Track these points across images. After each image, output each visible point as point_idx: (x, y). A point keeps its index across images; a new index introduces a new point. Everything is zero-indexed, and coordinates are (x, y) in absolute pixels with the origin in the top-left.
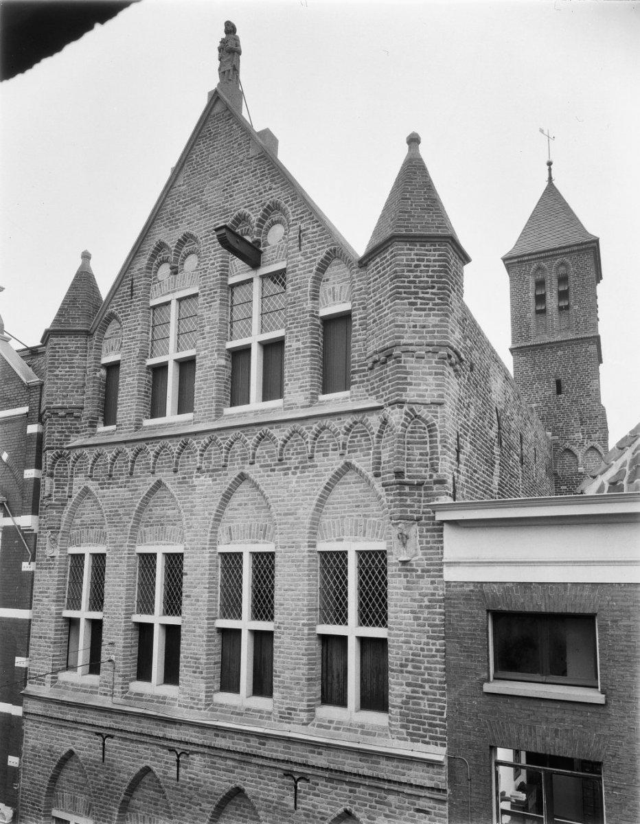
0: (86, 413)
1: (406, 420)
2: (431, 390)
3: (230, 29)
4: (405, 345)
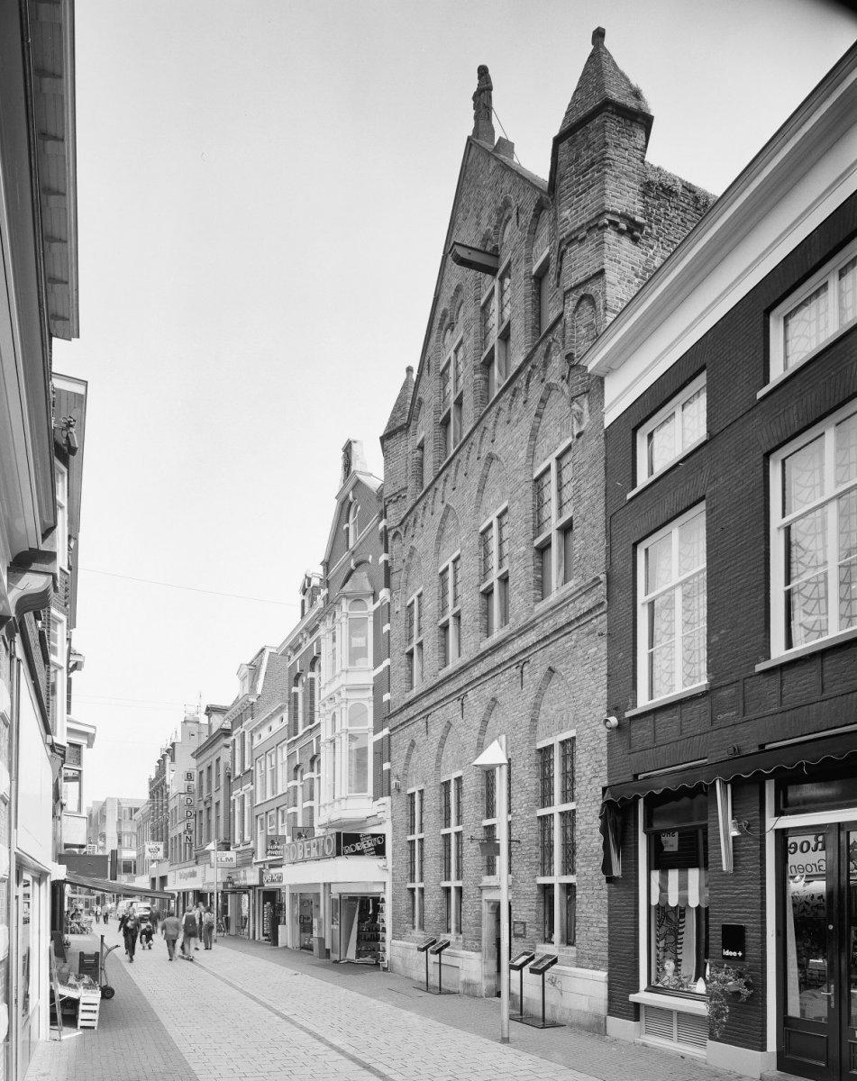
0: (409, 489)
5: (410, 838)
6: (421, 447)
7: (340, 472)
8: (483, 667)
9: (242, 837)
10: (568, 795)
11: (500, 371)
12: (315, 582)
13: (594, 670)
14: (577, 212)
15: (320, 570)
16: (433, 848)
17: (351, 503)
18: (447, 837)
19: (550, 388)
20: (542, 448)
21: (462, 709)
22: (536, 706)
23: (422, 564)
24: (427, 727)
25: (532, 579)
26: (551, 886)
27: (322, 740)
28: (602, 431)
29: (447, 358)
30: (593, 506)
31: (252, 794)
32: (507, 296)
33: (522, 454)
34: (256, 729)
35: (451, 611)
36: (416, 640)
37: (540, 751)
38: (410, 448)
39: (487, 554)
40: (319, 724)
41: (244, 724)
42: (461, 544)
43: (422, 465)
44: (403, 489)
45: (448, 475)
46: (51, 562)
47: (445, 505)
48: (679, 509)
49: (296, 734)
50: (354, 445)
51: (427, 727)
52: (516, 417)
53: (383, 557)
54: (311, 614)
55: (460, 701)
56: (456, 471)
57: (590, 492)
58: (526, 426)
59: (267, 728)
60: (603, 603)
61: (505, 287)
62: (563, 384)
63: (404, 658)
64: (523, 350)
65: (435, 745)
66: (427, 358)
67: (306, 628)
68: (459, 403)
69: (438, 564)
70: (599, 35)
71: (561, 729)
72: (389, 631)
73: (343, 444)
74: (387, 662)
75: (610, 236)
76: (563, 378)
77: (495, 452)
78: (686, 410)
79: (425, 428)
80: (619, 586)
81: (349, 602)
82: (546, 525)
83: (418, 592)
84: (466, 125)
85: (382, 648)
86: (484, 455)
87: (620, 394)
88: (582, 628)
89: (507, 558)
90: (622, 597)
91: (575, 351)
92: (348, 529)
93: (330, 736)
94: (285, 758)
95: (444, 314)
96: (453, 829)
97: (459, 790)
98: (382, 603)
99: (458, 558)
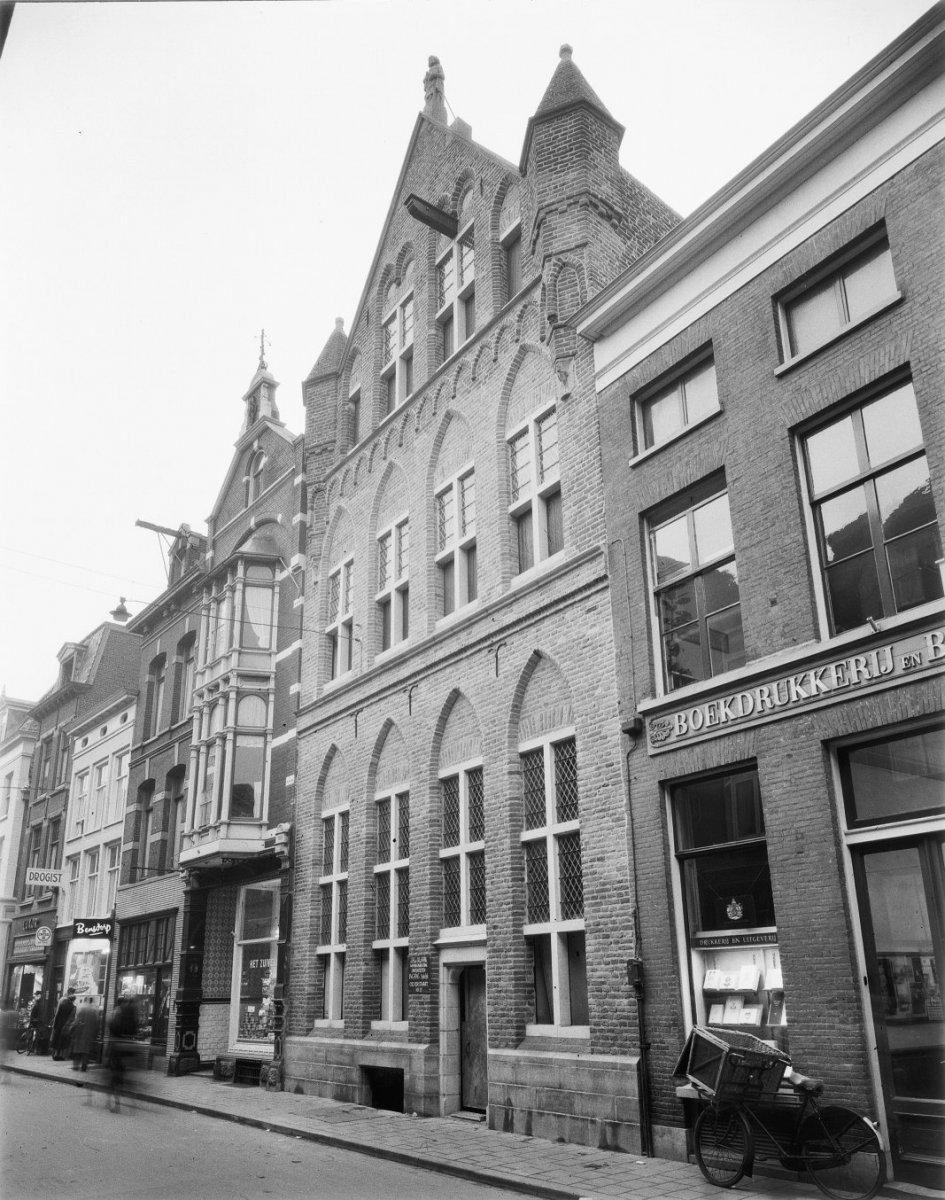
0: (338, 443)
1: (555, 270)
2: (575, 235)
3: (434, 62)
4: (547, 206)
5: (324, 880)
10: (568, 807)
29: (392, 312)
34: (81, 732)
36: (341, 618)
37: (524, 756)
42: (409, 502)
53: (298, 518)
55: (407, 694)
64: (492, 310)
68: (408, 358)
72: (302, 606)
76: (542, 339)
83: (347, 560)
84: (418, 103)
97: (404, 812)
99: (405, 522)
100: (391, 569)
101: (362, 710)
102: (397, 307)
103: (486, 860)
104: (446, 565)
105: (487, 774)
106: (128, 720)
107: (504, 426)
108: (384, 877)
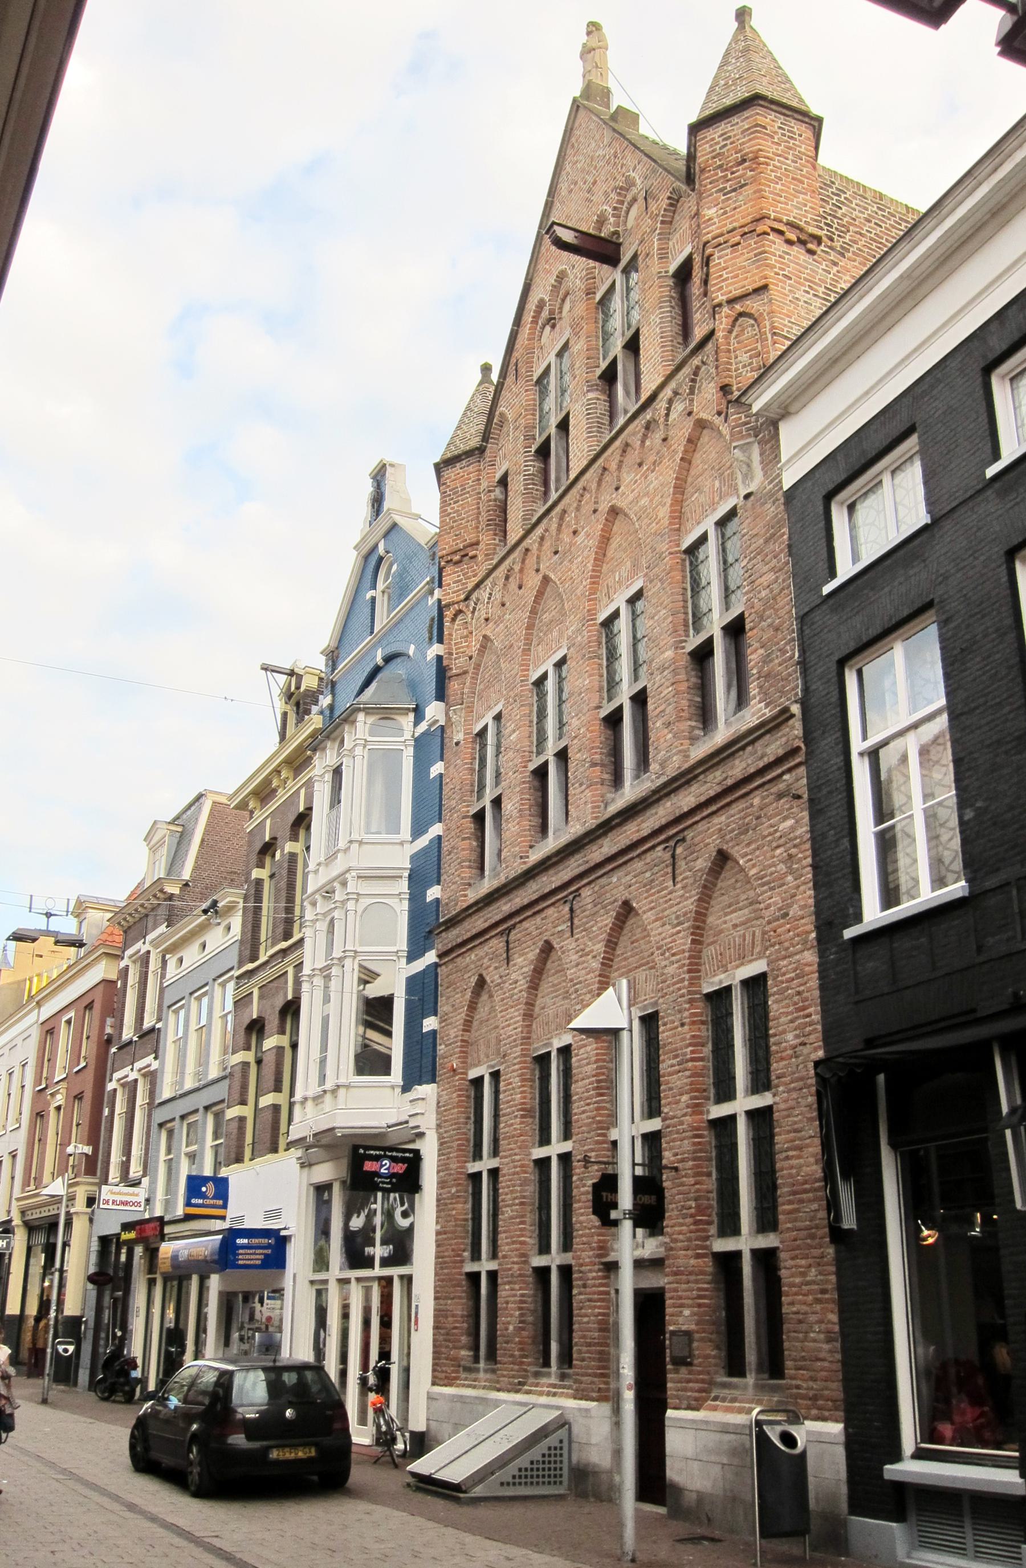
0: (481, 546)
6: (503, 482)
7: (364, 509)
8: (608, 846)
9: (125, 1167)
11: (627, 393)
12: (310, 682)
13: (790, 856)
14: (725, 213)
15: (320, 663)
16: (517, 1193)
17: (381, 559)
18: (543, 1164)
19: (701, 425)
20: (694, 500)
21: (572, 919)
22: (700, 916)
23: (503, 666)
24: (508, 951)
25: (685, 703)
26: (737, 1255)
27: (306, 970)
28: (781, 492)
30: (774, 599)
31: (152, 1077)
32: (634, 296)
33: (664, 512)
34: (174, 948)
35: (552, 747)
38: (484, 484)
39: (612, 655)
40: (301, 941)
41: (149, 938)
43: (505, 511)
44: (472, 545)
45: (564, 512)
46: (821, 1080)
47: (540, 576)
48: (873, 632)
49: (254, 958)
50: (389, 470)
51: (508, 951)
52: (652, 458)
53: (436, 650)
54: (299, 736)
56: (560, 525)
57: (771, 576)
58: (666, 475)
59: (195, 946)
60: (798, 748)
61: (632, 283)
62: (718, 420)
63: (469, 826)
65: (523, 984)
66: (513, 360)
67: (288, 762)
69: (526, 668)
70: (742, 15)
71: (743, 959)
72: (441, 775)
73: (372, 465)
74: (436, 830)
75: (777, 245)
77: (621, 504)
78: (897, 480)
79: (513, 455)
80: (824, 721)
81: (371, 719)
82: (705, 620)
85: (429, 804)
86: (604, 507)
87: (808, 441)
88: (766, 787)
89: (645, 667)
90: (828, 741)
91: (734, 381)
92: (373, 599)
93: (321, 964)
94: (229, 1006)
95: (541, 304)
96: (556, 1148)
97: (567, 1074)
98: (430, 726)
100: (714, 594)
101: (514, 926)
102: (552, 358)
103: (664, 1145)
104: (703, 655)
105: (665, 1024)
106: (232, 932)
107: (679, 530)
108: (725, 1126)
